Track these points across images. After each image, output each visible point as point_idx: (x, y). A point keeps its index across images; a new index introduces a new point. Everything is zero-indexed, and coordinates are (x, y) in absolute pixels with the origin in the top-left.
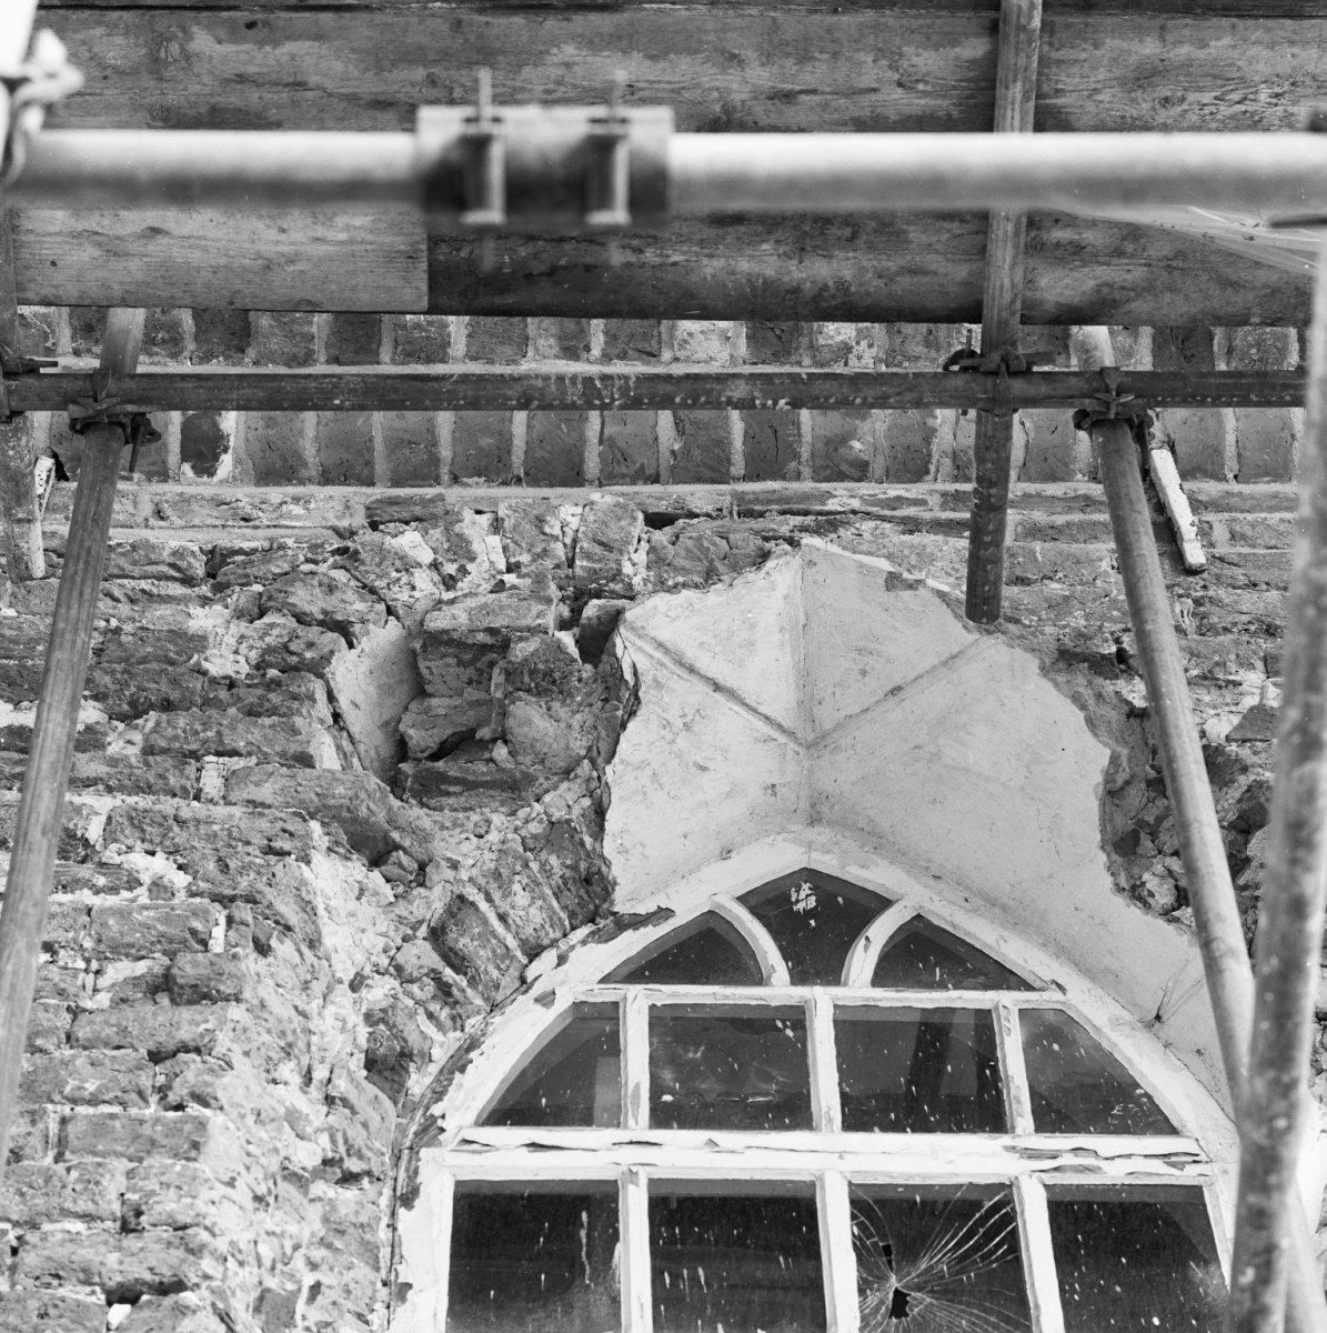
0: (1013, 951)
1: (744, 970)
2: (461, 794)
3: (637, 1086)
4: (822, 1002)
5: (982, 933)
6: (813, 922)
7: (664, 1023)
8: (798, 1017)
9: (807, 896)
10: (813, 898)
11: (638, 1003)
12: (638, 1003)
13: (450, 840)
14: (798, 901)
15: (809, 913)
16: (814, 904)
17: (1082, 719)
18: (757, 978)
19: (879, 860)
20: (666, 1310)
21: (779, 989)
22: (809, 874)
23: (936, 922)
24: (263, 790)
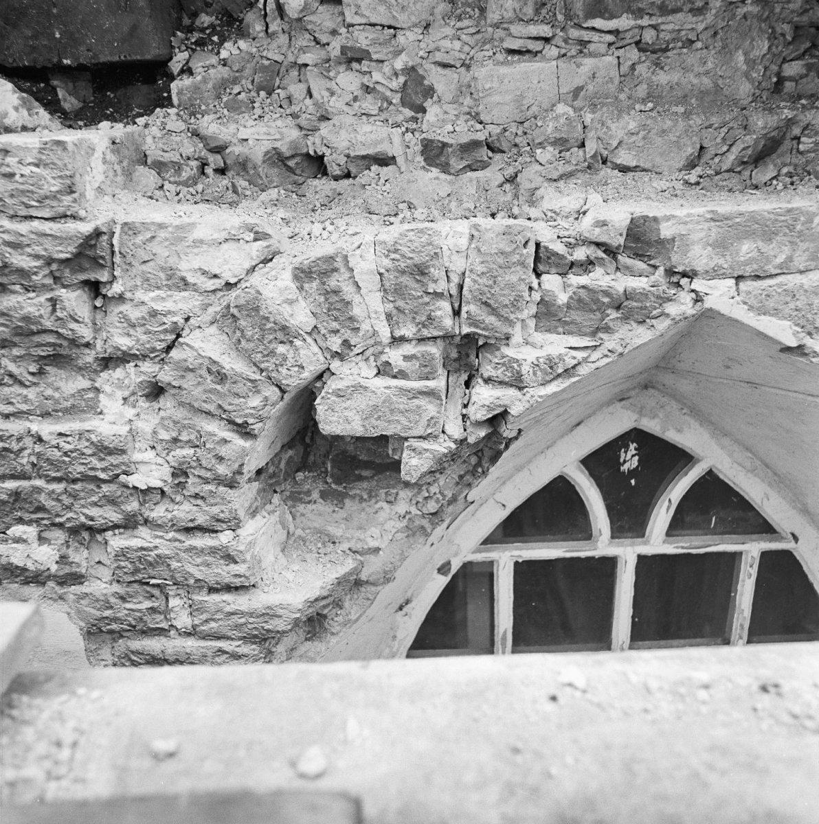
0: (771, 506)
1: (577, 524)
2: (372, 477)
3: (505, 632)
4: (628, 554)
5: (753, 489)
6: (633, 482)
7: (523, 570)
8: (609, 564)
9: (633, 456)
10: (637, 458)
11: (505, 559)
12: (505, 559)
13: (367, 509)
14: (625, 462)
15: (632, 473)
16: (636, 464)
17: (494, 468)
18: (677, 526)
19: (692, 421)
20: (332, 467)
21: (603, 544)
22: (637, 435)
23: (722, 477)
24: (96, 141)
